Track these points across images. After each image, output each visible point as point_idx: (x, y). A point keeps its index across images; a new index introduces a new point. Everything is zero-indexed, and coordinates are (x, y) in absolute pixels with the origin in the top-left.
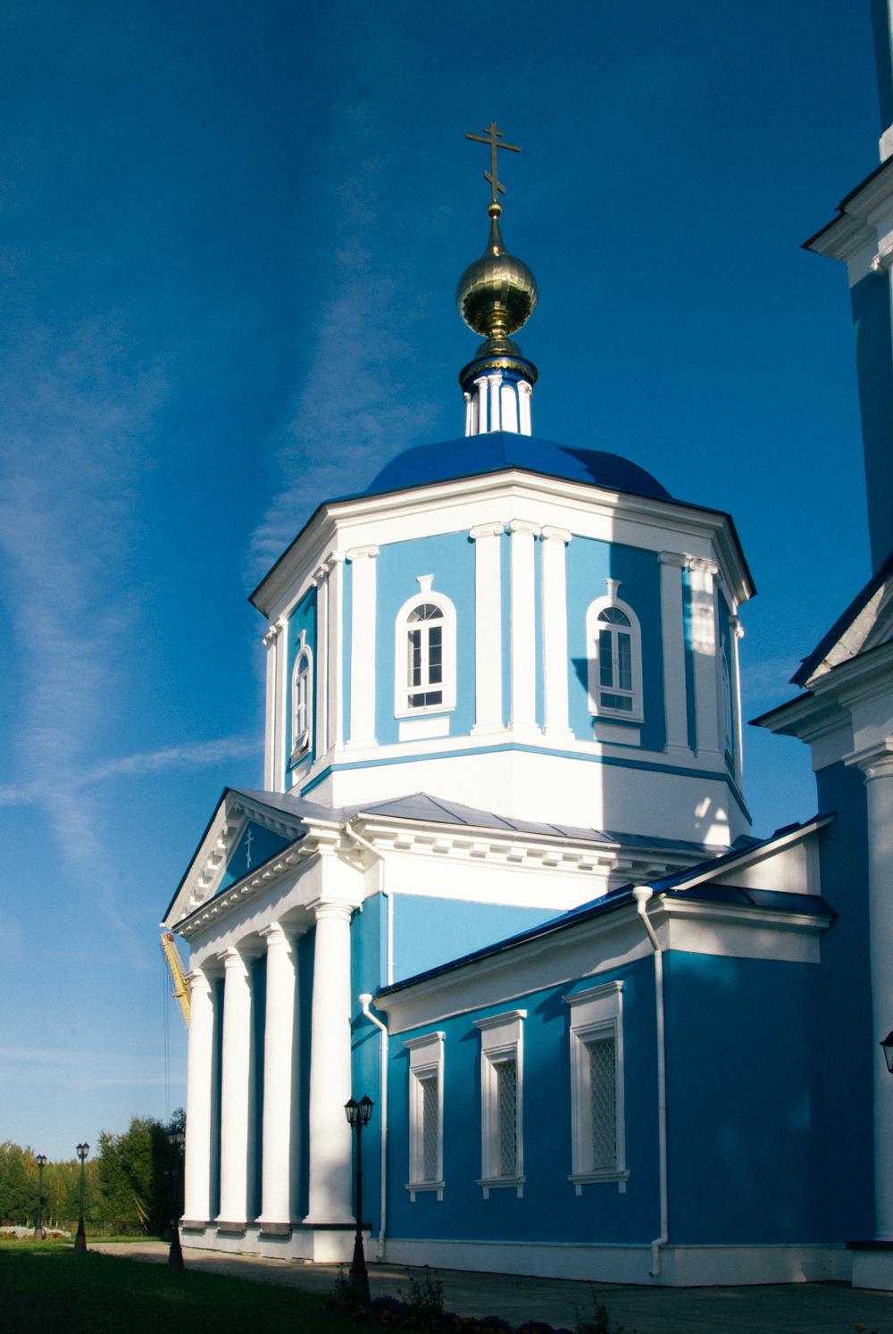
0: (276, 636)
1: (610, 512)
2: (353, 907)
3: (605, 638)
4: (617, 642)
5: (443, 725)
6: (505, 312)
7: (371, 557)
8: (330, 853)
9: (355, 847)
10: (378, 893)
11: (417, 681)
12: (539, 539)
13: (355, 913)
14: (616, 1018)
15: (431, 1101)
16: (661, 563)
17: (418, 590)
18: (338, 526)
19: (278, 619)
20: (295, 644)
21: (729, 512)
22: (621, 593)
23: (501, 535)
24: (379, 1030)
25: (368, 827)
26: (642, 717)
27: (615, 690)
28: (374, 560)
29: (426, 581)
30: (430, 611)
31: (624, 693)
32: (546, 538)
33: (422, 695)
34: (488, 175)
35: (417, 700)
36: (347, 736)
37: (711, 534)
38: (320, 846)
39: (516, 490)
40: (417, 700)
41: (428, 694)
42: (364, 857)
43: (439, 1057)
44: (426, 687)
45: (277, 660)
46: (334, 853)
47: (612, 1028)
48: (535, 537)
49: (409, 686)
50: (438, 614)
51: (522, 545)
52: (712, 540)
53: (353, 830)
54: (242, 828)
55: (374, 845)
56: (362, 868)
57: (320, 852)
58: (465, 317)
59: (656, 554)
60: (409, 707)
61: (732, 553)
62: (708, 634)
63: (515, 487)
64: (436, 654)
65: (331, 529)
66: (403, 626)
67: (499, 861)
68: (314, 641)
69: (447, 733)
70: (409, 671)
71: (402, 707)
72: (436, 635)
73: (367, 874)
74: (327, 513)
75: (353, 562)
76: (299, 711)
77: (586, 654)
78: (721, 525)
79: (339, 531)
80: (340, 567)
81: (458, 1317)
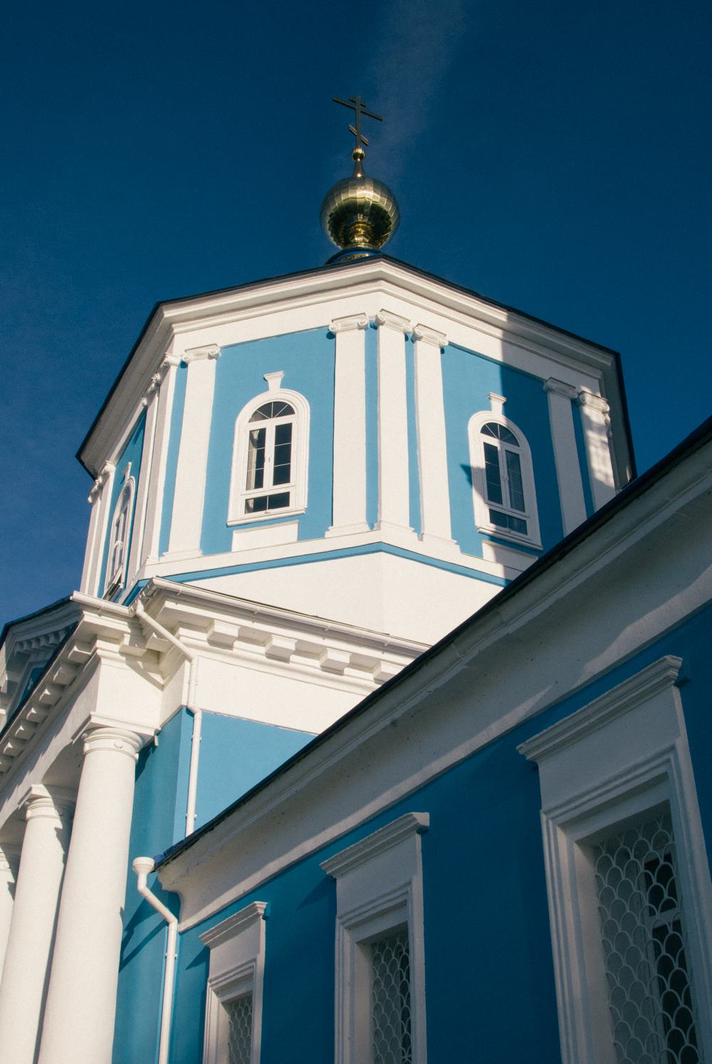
0: (101, 487)
2: (140, 735)
3: (490, 451)
5: (292, 529)
6: (368, 225)
7: (210, 357)
8: (111, 655)
9: (150, 645)
10: (181, 708)
11: (259, 483)
12: (411, 339)
13: (146, 751)
14: (672, 748)
15: (238, 1033)
16: (550, 390)
17: (267, 389)
18: (175, 331)
19: (105, 464)
20: (120, 479)
21: (617, 350)
22: (508, 410)
23: (365, 328)
24: (166, 923)
25: (169, 604)
27: (506, 507)
28: (214, 361)
29: (275, 380)
30: (281, 408)
31: (516, 514)
32: (420, 338)
33: (264, 498)
35: (260, 504)
36: (164, 547)
37: (599, 375)
38: (99, 643)
39: (383, 285)
40: (260, 504)
41: (271, 497)
42: (165, 664)
43: (258, 952)
44: (269, 488)
45: (101, 511)
46: (118, 656)
47: (663, 778)
48: (407, 338)
49: (248, 488)
50: (289, 410)
51: (390, 341)
53: (146, 610)
54: (23, 682)
55: (178, 638)
56: (161, 681)
57: (99, 652)
59: (540, 381)
62: (604, 464)
63: (382, 281)
64: (283, 455)
65: (168, 336)
66: (244, 425)
67: (363, 682)
68: (137, 471)
70: (249, 474)
71: (236, 512)
72: (284, 434)
73: (166, 689)
74: (163, 315)
75: (190, 365)
76: (115, 549)
77: (469, 460)
78: (609, 364)
79: (176, 337)
80: (173, 371)
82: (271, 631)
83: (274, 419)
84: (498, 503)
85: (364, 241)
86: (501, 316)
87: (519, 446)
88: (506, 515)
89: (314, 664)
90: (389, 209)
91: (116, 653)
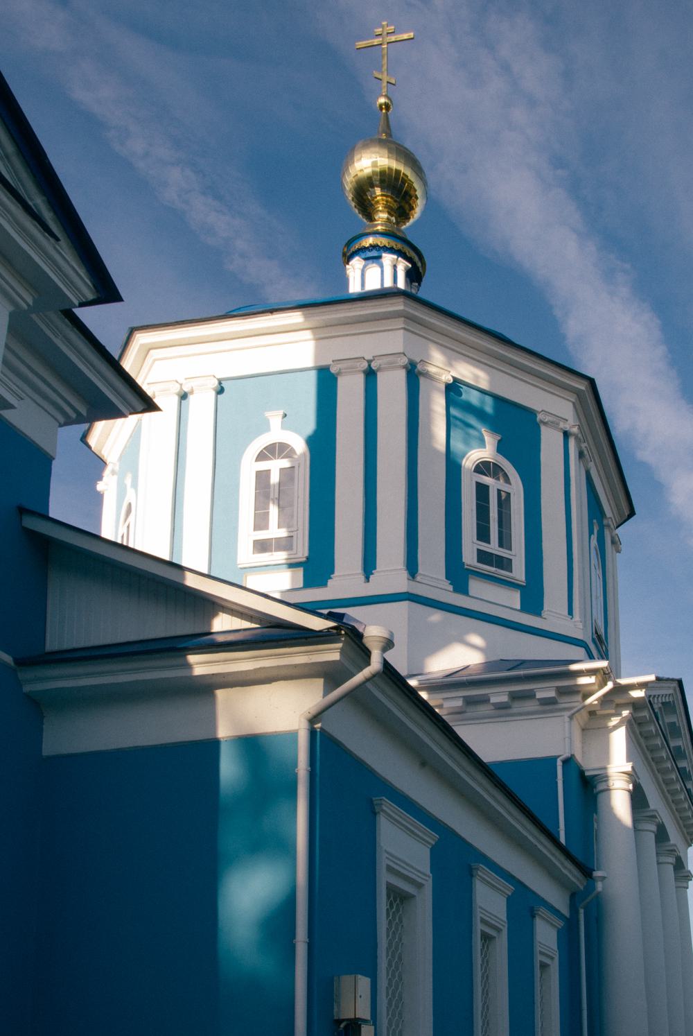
1: (308, 335)
4: (496, 516)
17: (268, 429)
22: (501, 448)
26: (523, 578)
27: (493, 547)
34: (377, 75)
52: (574, 403)
58: (359, 213)
60: (253, 553)
61: (597, 426)
69: (301, 585)
81: (43, 724)
82: (532, 688)
83: (279, 460)
84: (484, 542)
85: (383, 200)
86: (296, 317)
87: (510, 484)
88: (492, 554)
89: (530, 706)
90: (395, 165)
91: (197, 664)
